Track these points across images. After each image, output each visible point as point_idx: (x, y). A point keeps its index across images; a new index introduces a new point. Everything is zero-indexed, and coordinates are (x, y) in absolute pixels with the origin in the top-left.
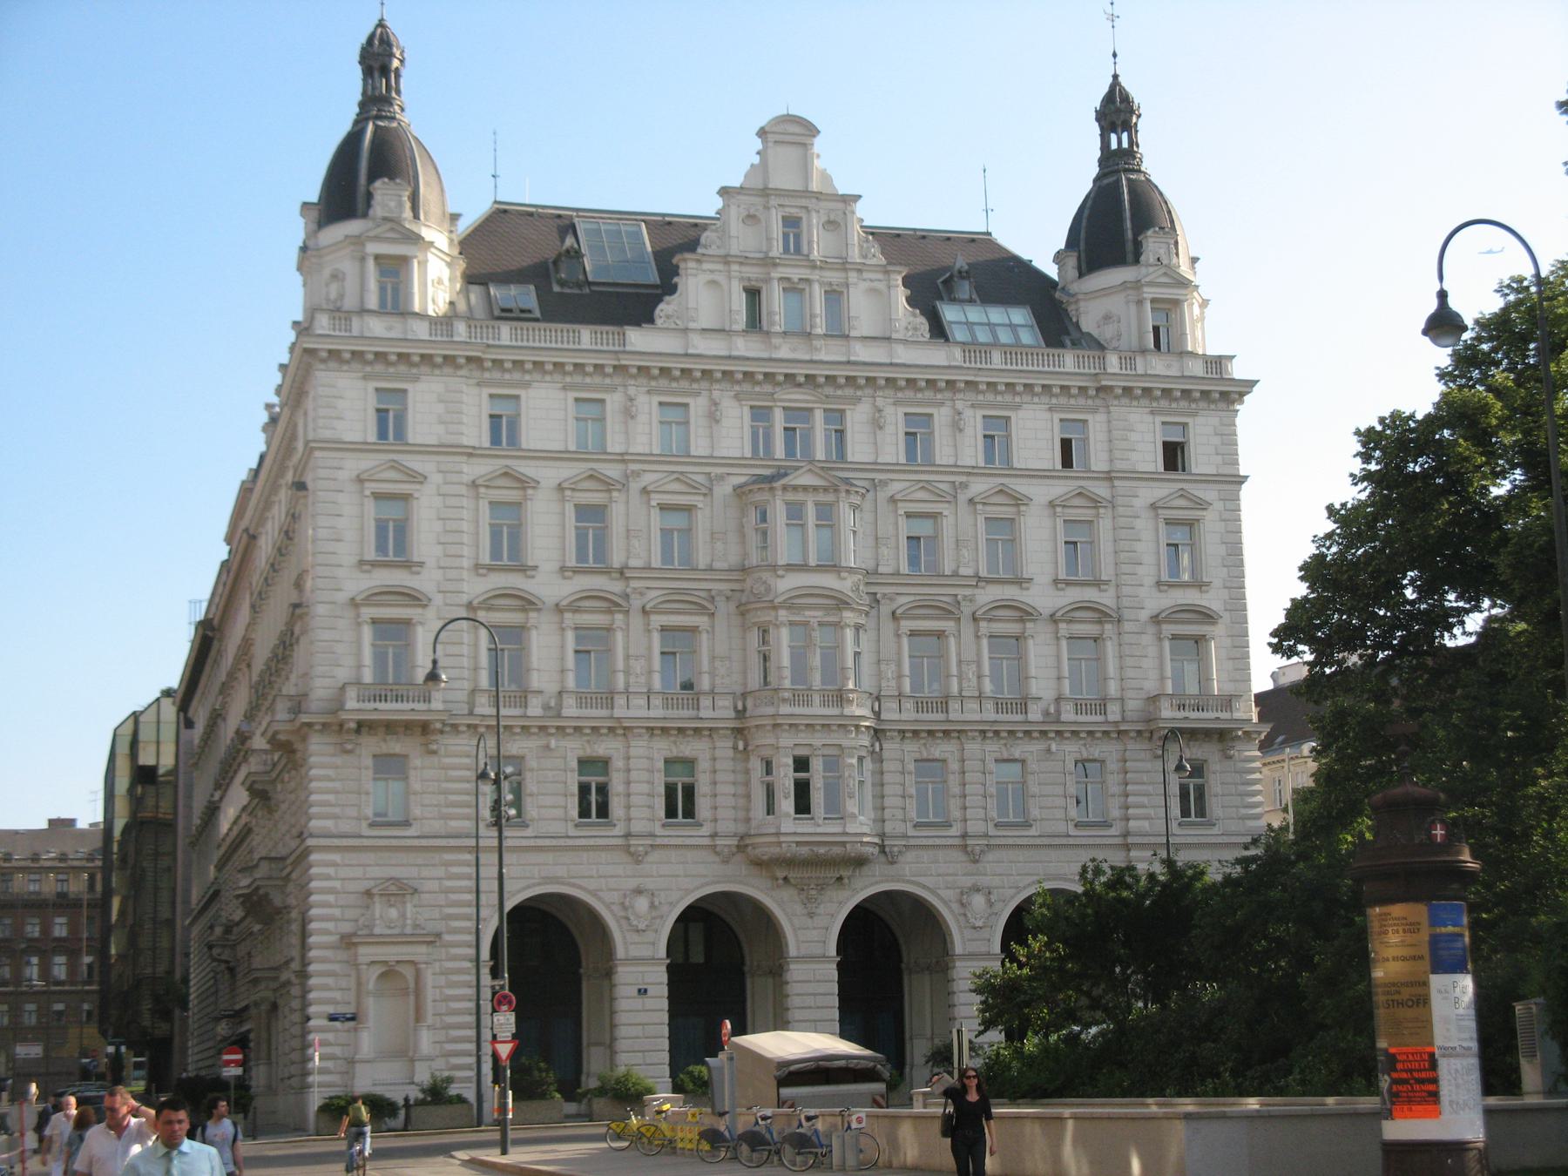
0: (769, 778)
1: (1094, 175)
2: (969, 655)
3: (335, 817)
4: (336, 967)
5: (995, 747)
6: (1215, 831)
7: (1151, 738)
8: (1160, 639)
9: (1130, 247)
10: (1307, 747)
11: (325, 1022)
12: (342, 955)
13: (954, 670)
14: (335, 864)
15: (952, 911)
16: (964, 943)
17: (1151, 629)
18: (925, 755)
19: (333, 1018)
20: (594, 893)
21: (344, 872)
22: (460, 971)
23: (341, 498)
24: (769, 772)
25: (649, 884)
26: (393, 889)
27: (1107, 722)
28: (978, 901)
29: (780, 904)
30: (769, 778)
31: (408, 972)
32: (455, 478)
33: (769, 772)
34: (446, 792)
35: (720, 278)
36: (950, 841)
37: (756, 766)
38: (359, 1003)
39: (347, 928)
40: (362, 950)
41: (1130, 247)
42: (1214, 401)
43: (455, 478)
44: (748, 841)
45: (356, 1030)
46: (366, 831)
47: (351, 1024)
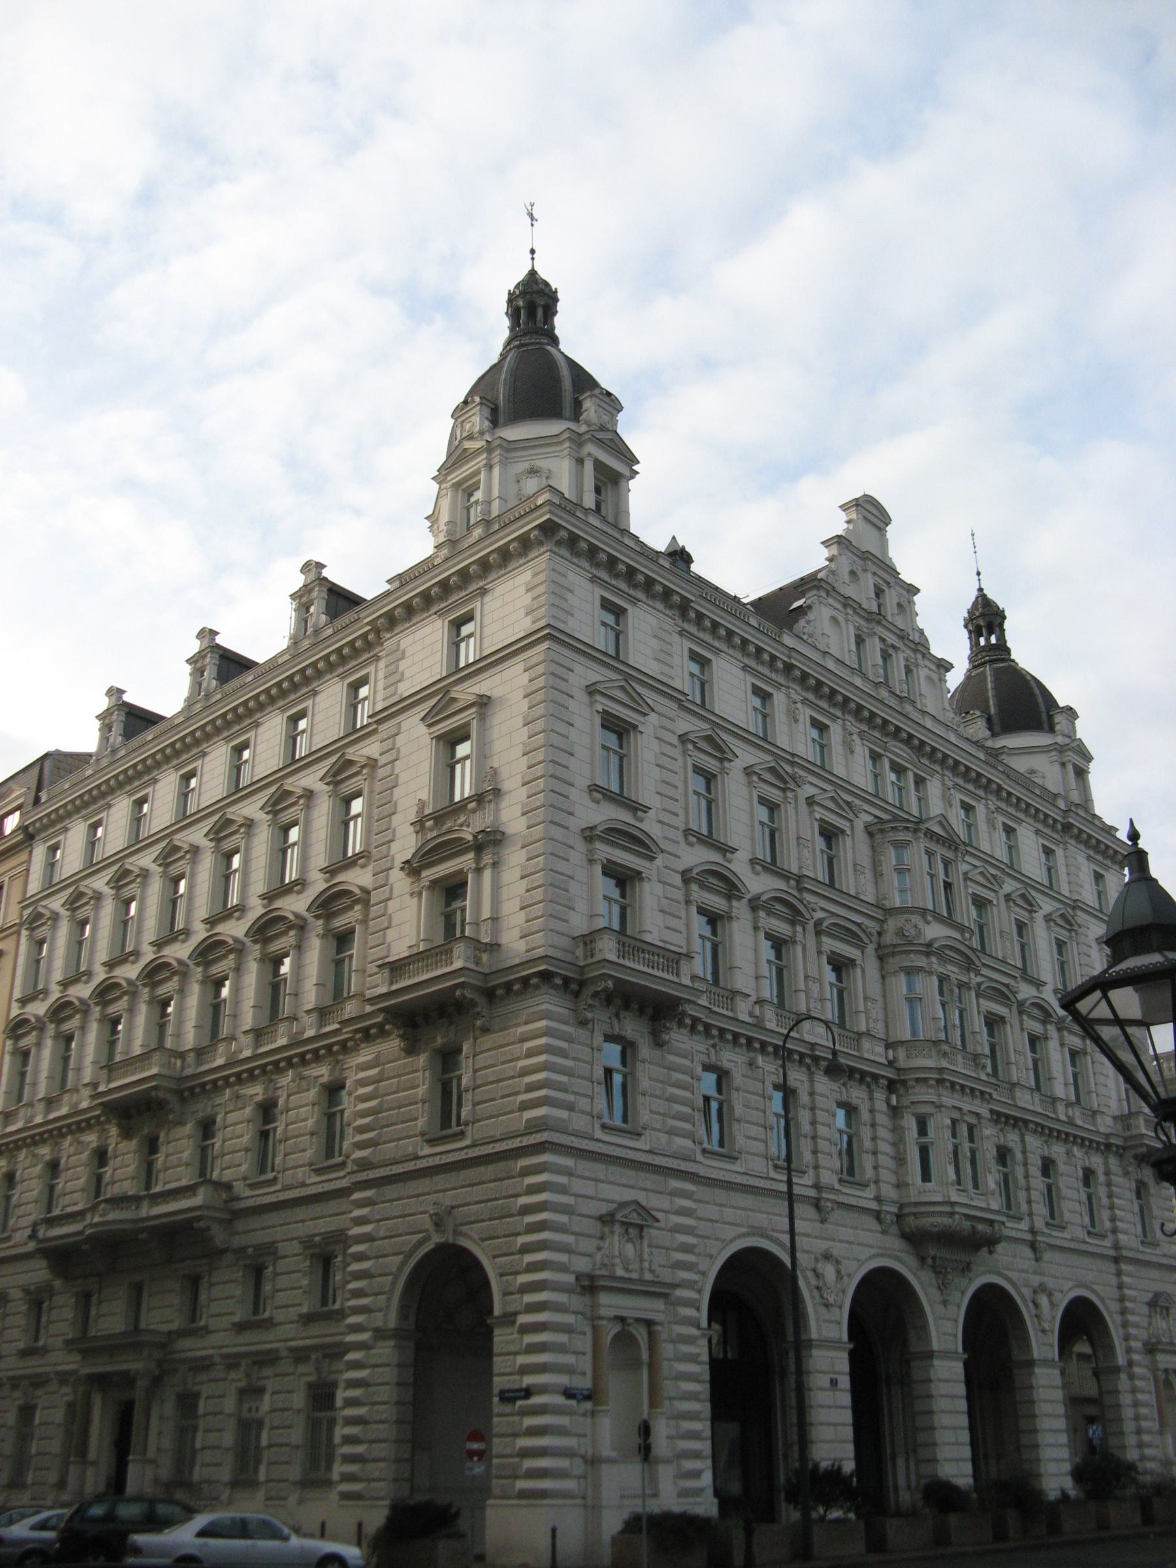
0: (924, 1140)
1: (559, 304)
2: (813, 972)
3: (570, 1107)
4: (569, 1319)
5: (702, 1048)
6: (737, 1167)
7: (577, 995)
8: (591, 861)
9: (1044, 717)
10: (667, 1037)
11: (560, 1400)
12: (577, 1302)
13: (802, 986)
14: (569, 1173)
15: (1029, 1311)
16: (819, 1327)
17: (581, 845)
18: (616, 1031)
19: (569, 1394)
20: (1102, 1300)
21: (578, 1186)
22: (690, 1340)
23: (572, 704)
24: (923, 1131)
25: (837, 1250)
26: (635, 1218)
27: (1097, 1132)
28: (1044, 1300)
29: (921, 1282)
30: (924, 1140)
31: (641, 1334)
32: (668, 724)
33: (923, 1131)
34: (671, 1099)
35: (841, 618)
36: (1019, 1235)
37: (910, 1123)
38: (596, 1378)
39: (582, 1265)
40: (604, 1298)
41: (1044, 717)
42: (578, 555)
43: (668, 724)
44: (906, 1210)
45: (593, 1414)
46: (599, 1134)
47: (588, 1405)
